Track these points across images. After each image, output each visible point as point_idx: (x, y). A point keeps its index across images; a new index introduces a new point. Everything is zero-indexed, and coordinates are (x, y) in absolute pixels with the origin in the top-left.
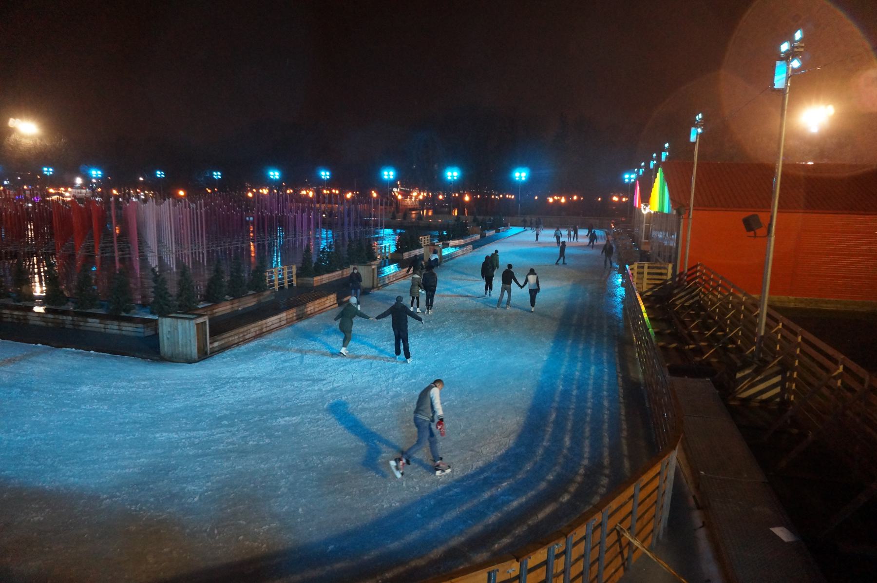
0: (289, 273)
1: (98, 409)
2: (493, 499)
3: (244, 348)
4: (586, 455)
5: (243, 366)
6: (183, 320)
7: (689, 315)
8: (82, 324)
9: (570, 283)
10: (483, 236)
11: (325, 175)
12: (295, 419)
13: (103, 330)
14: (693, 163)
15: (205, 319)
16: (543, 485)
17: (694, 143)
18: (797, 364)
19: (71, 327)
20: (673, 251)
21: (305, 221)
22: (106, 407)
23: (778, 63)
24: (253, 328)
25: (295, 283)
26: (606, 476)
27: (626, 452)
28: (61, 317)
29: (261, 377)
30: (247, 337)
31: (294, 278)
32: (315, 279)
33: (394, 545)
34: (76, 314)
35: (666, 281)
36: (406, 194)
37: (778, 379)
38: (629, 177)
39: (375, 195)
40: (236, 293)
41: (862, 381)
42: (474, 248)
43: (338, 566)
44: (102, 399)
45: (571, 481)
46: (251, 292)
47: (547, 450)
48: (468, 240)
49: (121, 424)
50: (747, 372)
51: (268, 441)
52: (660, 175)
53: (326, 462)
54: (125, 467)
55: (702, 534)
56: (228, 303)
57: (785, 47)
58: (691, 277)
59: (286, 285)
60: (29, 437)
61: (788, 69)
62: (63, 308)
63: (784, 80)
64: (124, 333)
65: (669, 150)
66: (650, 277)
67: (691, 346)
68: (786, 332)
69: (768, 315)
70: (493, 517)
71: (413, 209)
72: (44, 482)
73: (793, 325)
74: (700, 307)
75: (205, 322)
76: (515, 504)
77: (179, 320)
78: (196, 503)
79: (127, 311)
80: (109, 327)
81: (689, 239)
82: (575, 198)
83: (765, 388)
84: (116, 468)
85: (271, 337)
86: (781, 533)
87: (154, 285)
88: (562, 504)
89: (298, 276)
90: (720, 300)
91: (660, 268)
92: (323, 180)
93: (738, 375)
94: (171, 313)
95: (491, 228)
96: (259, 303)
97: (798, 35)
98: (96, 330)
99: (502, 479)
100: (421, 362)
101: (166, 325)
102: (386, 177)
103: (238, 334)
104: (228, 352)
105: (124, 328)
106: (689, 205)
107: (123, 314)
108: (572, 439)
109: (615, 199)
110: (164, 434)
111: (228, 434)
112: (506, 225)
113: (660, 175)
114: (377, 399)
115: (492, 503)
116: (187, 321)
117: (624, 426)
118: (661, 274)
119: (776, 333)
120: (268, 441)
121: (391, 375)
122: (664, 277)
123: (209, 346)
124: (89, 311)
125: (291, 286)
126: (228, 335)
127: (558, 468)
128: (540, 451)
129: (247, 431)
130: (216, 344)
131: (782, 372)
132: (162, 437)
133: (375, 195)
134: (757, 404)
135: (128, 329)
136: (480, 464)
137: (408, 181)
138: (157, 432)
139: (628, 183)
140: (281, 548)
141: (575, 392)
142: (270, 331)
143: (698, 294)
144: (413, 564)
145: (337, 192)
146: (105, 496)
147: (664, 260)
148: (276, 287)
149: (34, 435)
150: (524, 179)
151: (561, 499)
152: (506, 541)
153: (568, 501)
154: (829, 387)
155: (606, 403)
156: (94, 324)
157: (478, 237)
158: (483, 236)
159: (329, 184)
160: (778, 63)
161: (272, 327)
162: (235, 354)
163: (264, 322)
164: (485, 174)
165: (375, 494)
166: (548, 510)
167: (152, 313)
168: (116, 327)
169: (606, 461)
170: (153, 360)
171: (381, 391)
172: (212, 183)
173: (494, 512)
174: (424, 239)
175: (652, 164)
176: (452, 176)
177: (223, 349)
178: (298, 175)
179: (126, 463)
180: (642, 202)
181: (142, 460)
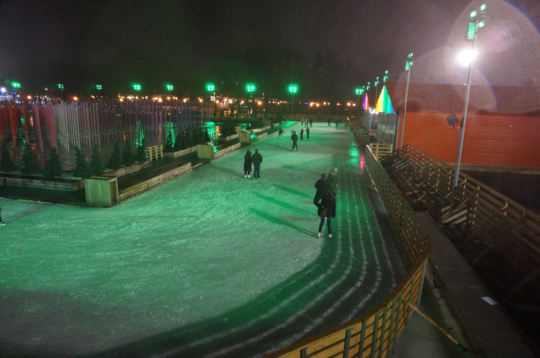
0: (158, 150)
1: (53, 238)
2: (316, 286)
3: (139, 197)
4: (365, 258)
5: (141, 209)
6: (101, 181)
7: (405, 175)
8: (29, 183)
9: (331, 155)
10: (272, 127)
11: (170, 87)
12: (183, 241)
13: (44, 188)
14: (407, 84)
15: (115, 179)
16: (344, 277)
17: (407, 71)
18: (476, 203)
19: (22, 186)
20: (393, 137)
21: (157, 117)
22: (58, 237)
23: (470, 24)
24: (143, 185)
25: (162, 156)
26: (379, 270)
27: (387, 256)
28: (14, 179)
29: (155, 215)
30: (140, 190)
31: (162, 153)
32: (175, 153)
33: (264, 316)
34: (23, 177)
35: (389, 154)
36: (221, 100)
37: (465, 212)
38: (359, 91)
39: (201, 101)
40: (128, 163)
41: (521, 213)
42: (268, 134)
43: (233, 330)
44: (55, 231)
45: (359, 274)
46: (136, 162)
47: (341, 256)
48: (264, 129)
49: (71, 248)
50: (448, 208)
51: (169, 255)
52: (384, 90)
53: (209, 267)
54: (81, 275)
55: (441, 302)
56: (123, 169)
57: (473, 14)
58: (405, 152)
59: (157, 157)
60: (11, 258)
61: (476, 27)
62: (13, 173)
63: (474, 34)
64: (58, 189)
65: (388, 75)
66: (380, 152)
67: (410, 193)
68: (468, 184)
69: (460, 176)
70: (319, 297)
71: (225, 110)
72: (29, 287)
73: (474, 180)
74: (410, 169)
75: (115, 182)
76: (330, 289)
77: (99, 180)
78: (133, 296)
79: (58, 175)
80: (48, 185)
81: (403, 129)
82: (325, 103)
83: (458, 217)
84: (76, 275)
85: (155, 190)
86: (487, 300)
87: (76, 158)
88: (358, 288)
89: (164, 151)
90: (423, 166)
91: (385, 147)
92: (169, 91)
93: (443, 210)
94: (92, 176)
95: (277, 121)
96: (142, 169)
97: (483, 7)
98: (39, 187)
99: (319, 274)
100: (253, 204)
101: (89, 184)
102: (209, 89)
103: (135, 188)
104: (129, 200)
105: (58, 186)
106: (403, 109)
107: (56, 177)
108: (354, 249)
109: (349, 104)
110: (101, 253)
111: (143, 252)
112: (285, 120)
113: (384, 90)
114: (231, 228)
115: (318, 289)
116: (104, 181)
117: (383, 241)
118: (386, 150)
119: (463, 185)
120: (169, 255)
121: (236, 213)
122: (388, 152)
123: (118, 197)
124: (32, 175)
125: (159, 158)
126: (128, 189)
127: (350, 267)
128: (338, 257)
129: (155, 249)
130: (122, 195)
131: (468, 208)
132: (100, 255)
133: (201, 101)
134: (454, 227)
135: (61, 186)
136: (304, 265)
137: (221, 92)
138: (96, 252)
139: (358, 95)
140: (194, 321)
141: (349, 221)
142: (153, 187)
143: (408, 162)
144: (278, 327)
145: (176, 98)
146: (73, 294)
147: (386, 141)
148: (151, 159)
149: (14, 257)
150: (295, 91)
151: (356, 285)
152: (330, 311)
153: (361, 286)
154: (499, 217)
155: (369, 227)
156: (37, 183)
157: (269, 127)
158: (272, 127)
159: (172, 93)
160: (470, 24)
161: (155, 184)
162: (134, 201)
163: (150, 181)
164: (272, 88)
165: (245, 285)
166: (350, 291)
167: (77, 176)
168: (53, 186)
169: (377, 262)
170: (81, 206)
171: (233, 223)
172: (96, 92)
173: (318, 294)
174: (238, 129)
175: (376, 83)
176: (251, 89)
177: (126, 198)
178: (153, 87)
179: (81, 272)
180: (370, 106)
181: (91, 270)
